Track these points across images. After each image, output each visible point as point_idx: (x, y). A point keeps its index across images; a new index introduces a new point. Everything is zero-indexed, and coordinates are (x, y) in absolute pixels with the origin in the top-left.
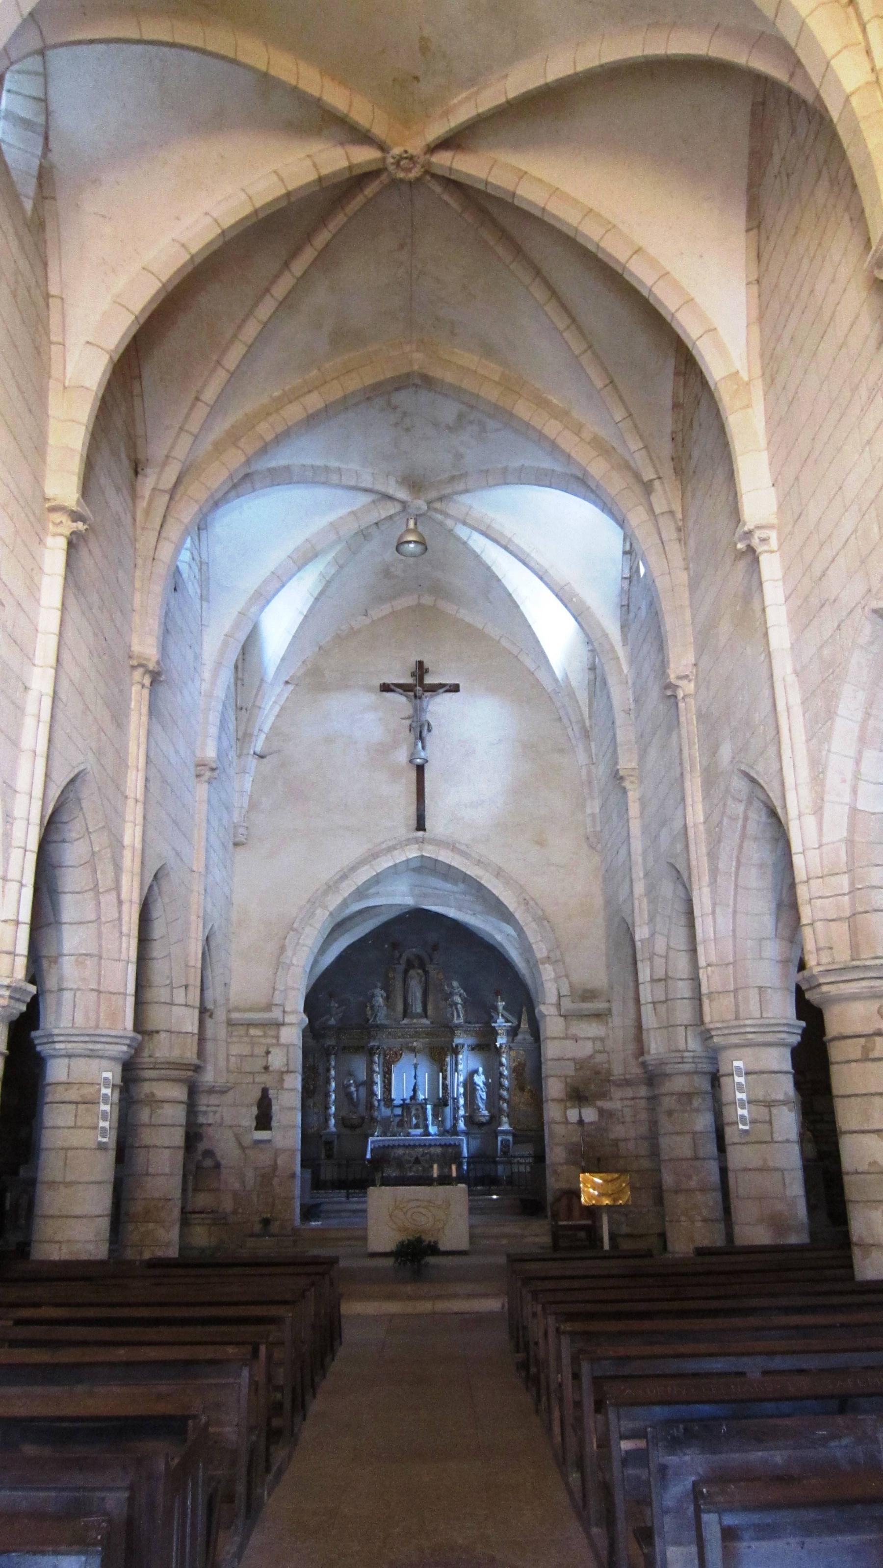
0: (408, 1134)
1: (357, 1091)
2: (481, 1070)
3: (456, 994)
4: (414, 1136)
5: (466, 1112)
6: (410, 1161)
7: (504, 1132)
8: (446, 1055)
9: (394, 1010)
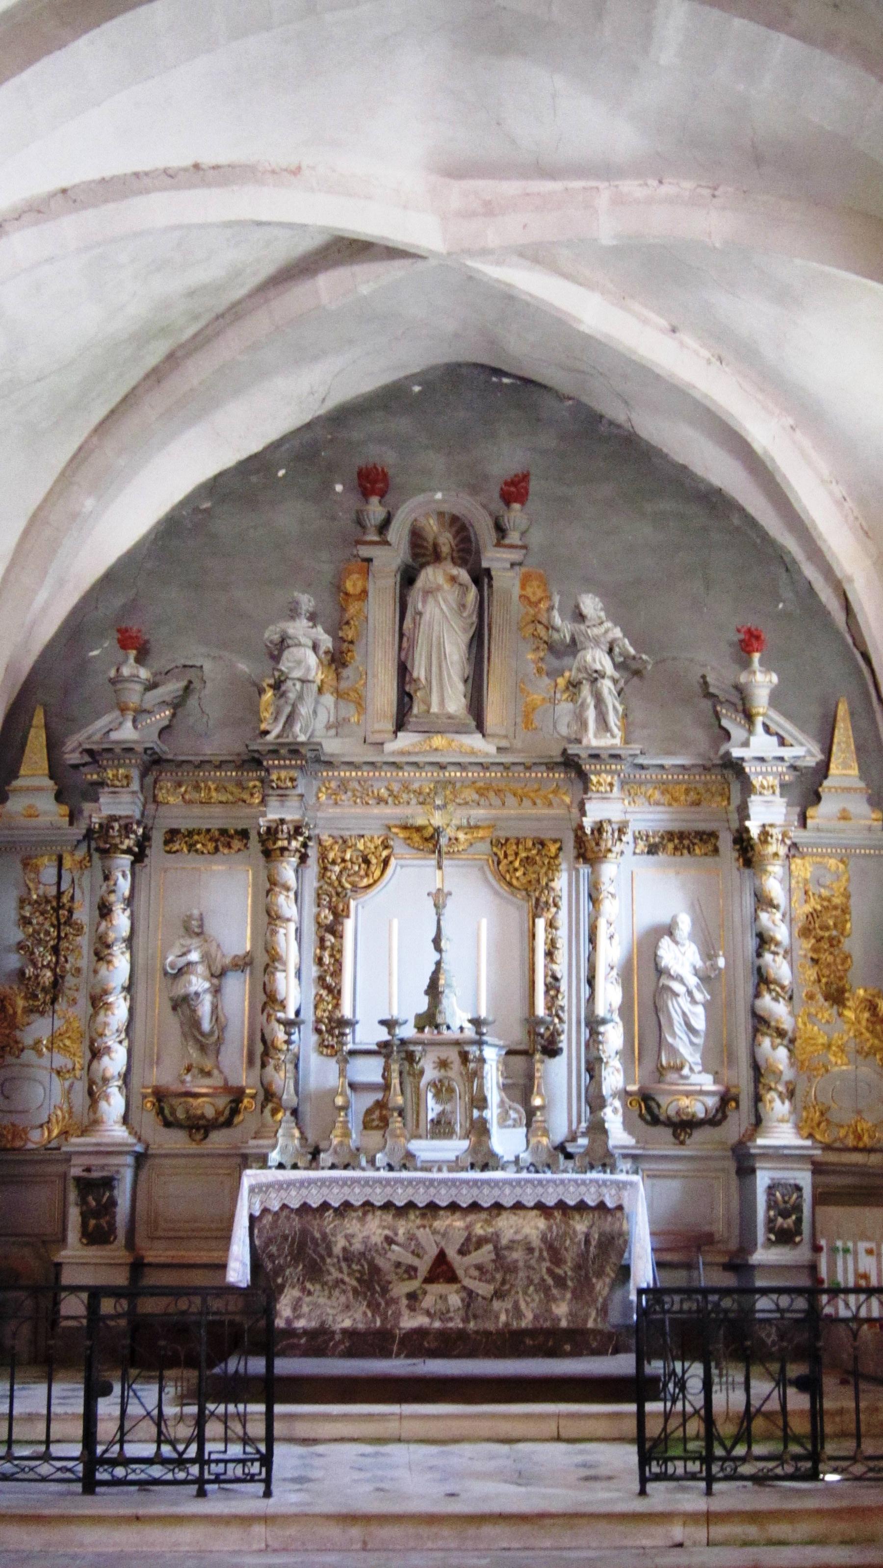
0: (408, 1161)
1: (216, 991)
2: (685, 924)
3: (596, 642)
4: (426, 1167)
5: (628, 1079)
6: (411, 1271)
7: (779, 1155)
8: (552, 868)
9: (360, 705)
